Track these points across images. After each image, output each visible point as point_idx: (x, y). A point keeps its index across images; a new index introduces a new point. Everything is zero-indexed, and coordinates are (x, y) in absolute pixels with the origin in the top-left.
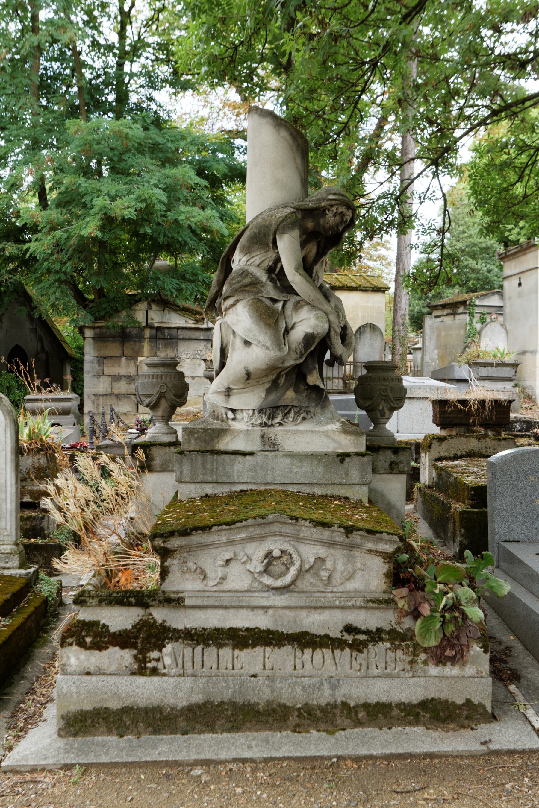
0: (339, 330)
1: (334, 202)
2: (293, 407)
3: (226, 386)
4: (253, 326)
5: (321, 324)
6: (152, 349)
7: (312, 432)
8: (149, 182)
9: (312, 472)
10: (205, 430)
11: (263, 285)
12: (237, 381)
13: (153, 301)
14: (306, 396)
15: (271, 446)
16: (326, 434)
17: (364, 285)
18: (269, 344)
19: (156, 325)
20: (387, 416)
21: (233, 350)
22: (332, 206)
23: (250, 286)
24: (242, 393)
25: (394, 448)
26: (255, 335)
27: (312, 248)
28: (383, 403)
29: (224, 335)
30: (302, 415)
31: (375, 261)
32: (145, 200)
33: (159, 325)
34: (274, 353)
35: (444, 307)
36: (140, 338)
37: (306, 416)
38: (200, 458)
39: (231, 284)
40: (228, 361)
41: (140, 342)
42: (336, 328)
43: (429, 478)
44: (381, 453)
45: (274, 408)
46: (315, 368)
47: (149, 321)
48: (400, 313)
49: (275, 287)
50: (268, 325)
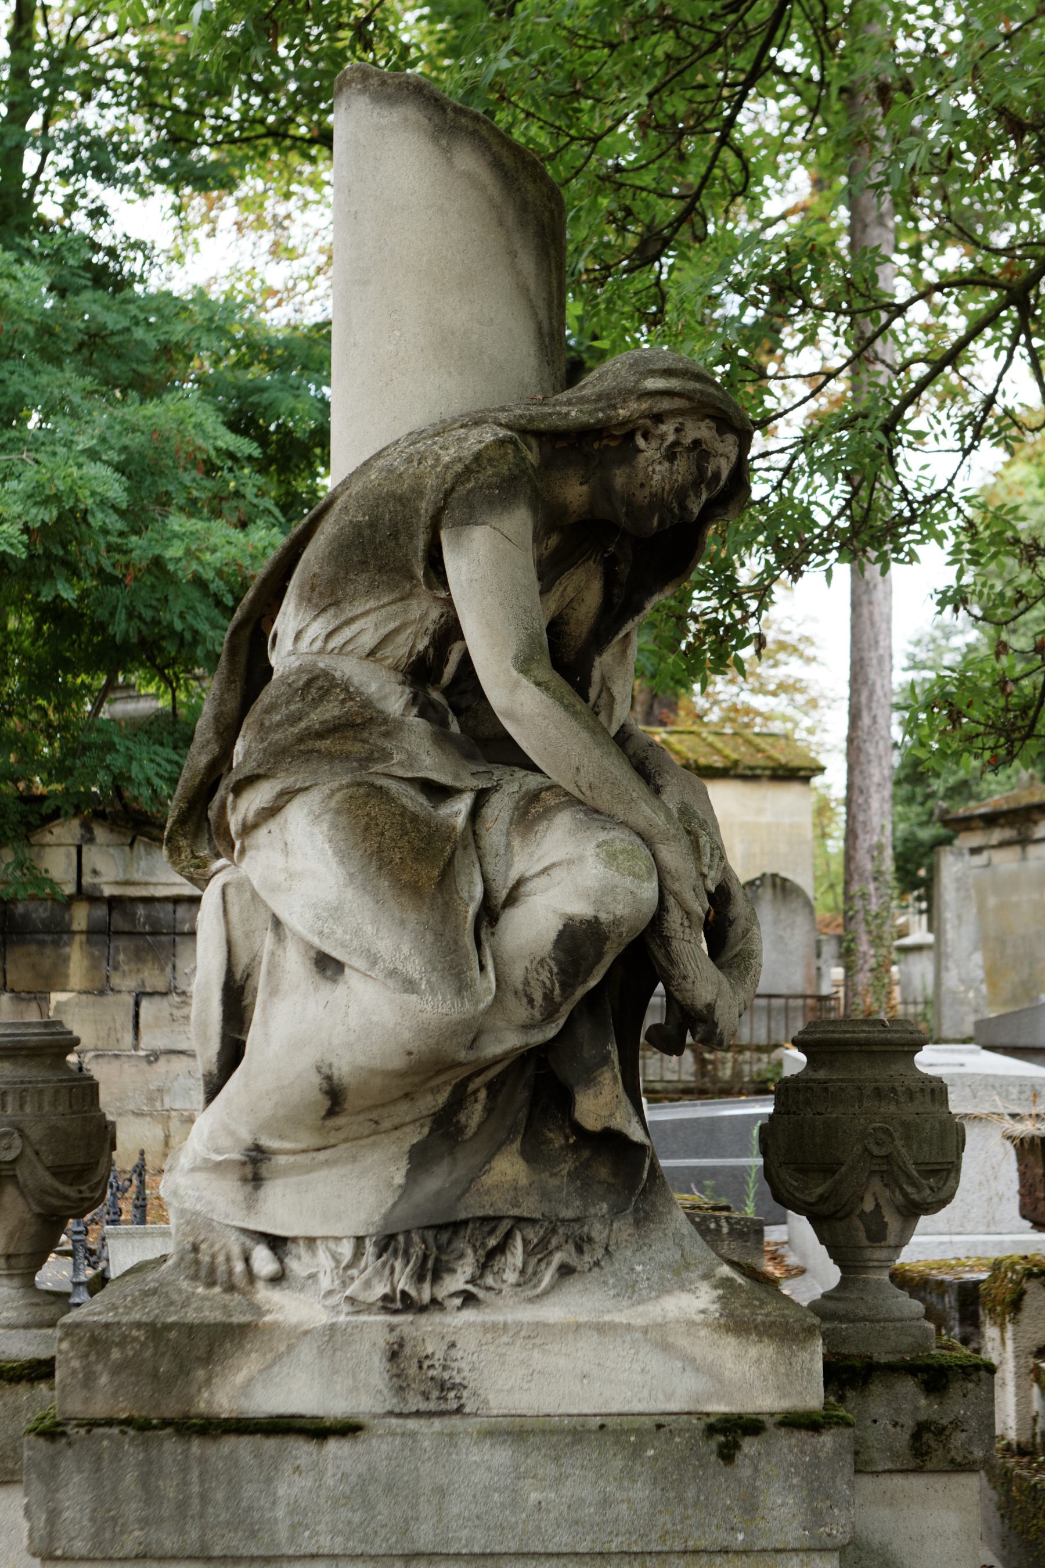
0: (699, 906)
1: (665, 404)
2: (519, 1220)
3: (246, 1137)
4: (349, 894)
5: (628, 882)
6: (94, 966)
7: (601, 1329)
8: (69, 444)
9: (606, 1502)
10: (156, 1331)
11: (391, 728)
12: (287, 1121)
13: (100, 816)
14: (572, 1175)
15: (429, 1391)
16: (659, 1338)
17: (749, 761)
18: (414, 968)
19: (108, 891)
20: (892, 1239)
21: (274, 992)
22: (658, 418)
23: (337, 734)
24: (309, 1169)
25: (927, 1368)
26: (357, 932)
27: (585, 590)
28: (876, 1185)
29: (237, 934)
30: (557, 1258)
31: (774, 694)
32: (56, 498)
33: (117, 891)
34: (436, 1007)
35: (991, 820)
36: (58, 931)
37: (573, 1260)
38: (132, 1452)
39: (263, 730)
40: (254, 1038)
41: (57, 944)
42: (689, 896)
43: (1020, 1418)
44: (876, 1388)
45: (440, 1228)
46: (606, 1060)
47: (87, 879)
48: (865, 842)
49: (442, 737)
50: (411, 890)
